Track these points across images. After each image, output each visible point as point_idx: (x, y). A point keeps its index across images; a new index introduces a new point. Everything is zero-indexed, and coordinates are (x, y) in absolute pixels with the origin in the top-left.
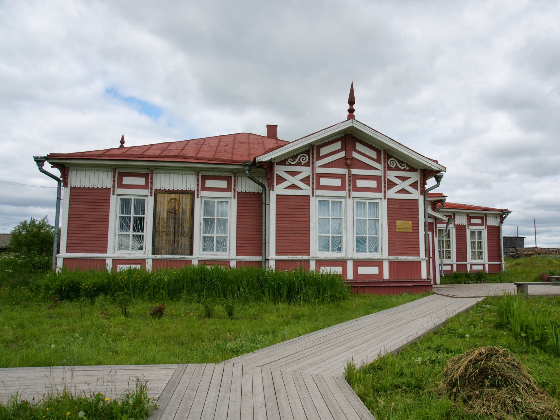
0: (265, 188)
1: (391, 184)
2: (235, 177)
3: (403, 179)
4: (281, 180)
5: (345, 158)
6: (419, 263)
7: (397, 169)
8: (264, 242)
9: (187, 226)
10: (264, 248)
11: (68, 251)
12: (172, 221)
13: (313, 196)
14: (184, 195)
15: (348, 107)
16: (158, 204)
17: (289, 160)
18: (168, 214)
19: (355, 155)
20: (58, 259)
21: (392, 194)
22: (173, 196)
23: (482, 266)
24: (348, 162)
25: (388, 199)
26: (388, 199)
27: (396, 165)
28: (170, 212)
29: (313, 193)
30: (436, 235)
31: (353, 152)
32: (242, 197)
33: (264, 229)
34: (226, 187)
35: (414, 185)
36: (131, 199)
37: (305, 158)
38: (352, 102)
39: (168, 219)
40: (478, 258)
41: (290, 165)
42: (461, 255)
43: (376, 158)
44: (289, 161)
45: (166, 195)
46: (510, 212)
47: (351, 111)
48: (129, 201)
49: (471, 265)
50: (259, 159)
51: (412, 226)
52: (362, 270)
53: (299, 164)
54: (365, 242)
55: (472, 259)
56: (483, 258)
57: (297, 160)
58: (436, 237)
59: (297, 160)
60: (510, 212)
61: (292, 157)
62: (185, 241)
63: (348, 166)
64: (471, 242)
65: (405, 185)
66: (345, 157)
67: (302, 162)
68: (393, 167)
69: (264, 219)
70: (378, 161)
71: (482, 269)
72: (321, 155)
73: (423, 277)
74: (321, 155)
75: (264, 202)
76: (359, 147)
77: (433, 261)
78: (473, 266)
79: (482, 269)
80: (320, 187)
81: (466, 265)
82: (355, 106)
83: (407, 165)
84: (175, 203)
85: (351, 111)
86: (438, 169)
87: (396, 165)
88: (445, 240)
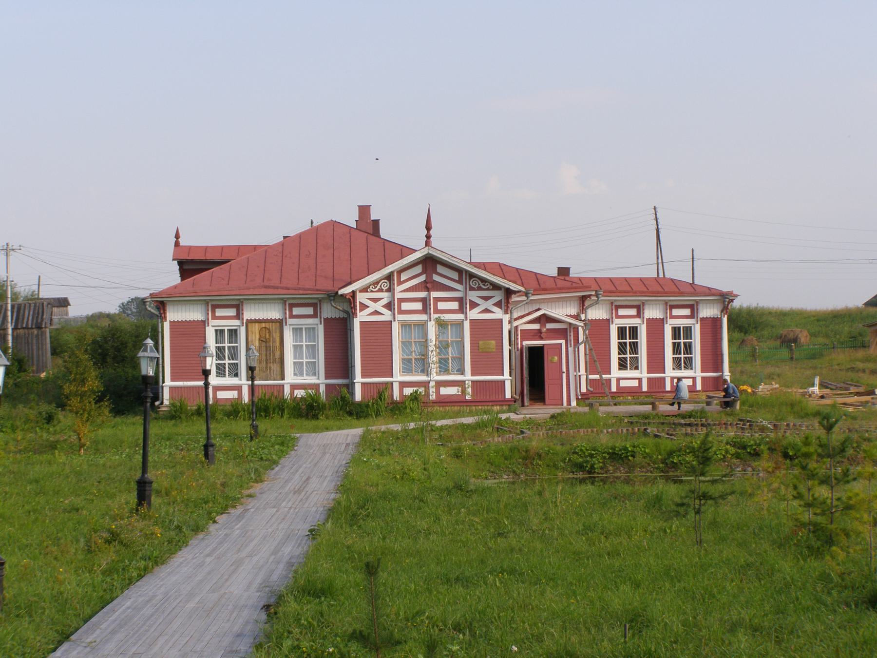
0: (349, 314)
1: (474, 305)
2: (320, 304)
3: (486, 299)
4: (364, 307)
5: (425, 282)
6: (503, 382)
7: (479, 289)
8: (350, 366)
9: (278, 354)
10: (350, 371)
11: (172, 380)
12: (264, 349)
13: (395, 321)
14: (274, 324)
15: (426, 232)
16: (250, 333)
17: (371, 287)
18: (259, 343)
19: (436, 278)
20: (164, 388)
21: (474, 314)
22: (263, 325)
23: (637, 381)
24: (427, 286)
25: (470, 320)
26: (470, 320)
27: (479, 284)
28: (262, 341)
29: (394, 318)
30: (571, 345)
31: (434, 275)
32: (328, 322)
33: (350, 353)
34: (312, 313)
35: (498, 304)
36: (224, 330)
37: (386, 284)
38: (428, 227)
39: (260, 347)
40: (684, 367)
41: (372, 291)
42: (656, 363)
43: (457, 279)
44: (371, 288)
45: (257, 324)
46: (736, 296)
47: (428, 237)
48: (222, 331)
49: (618, 380)
50: (341, 292)
51: (496, 346)
52: (444, 391)
53: (381, 290)
54: (449, 360)
55: (674, 369)
56: (694, 368)
57: (378, 287)
58: (571, 346)
59: (378, 287)
60: (736, 296)
61: (374, 284)
62: (275, 367)
63: (428, 290)
64: (674, 344)
65: (489, 304)
66: (425, 280)
67: (383, 288)
68: (475, 287)
69: (349, 345)
70: (460, 282)
71: (637, 385)
72: (402, 280)
73: (507, 397)
74: (402, 280)
75: (349, 328)
76: (440, 269)
77: (566, 376)
78: (218, 393)
79: (637, 385)
80: (401, 312)
81: (664, 379)
82: (432, 232)
83: (491, 284)
84: (266, 331)
85: (428, 237)
86: (517, 290)
87: (479, 284)
88: (630, 342)
